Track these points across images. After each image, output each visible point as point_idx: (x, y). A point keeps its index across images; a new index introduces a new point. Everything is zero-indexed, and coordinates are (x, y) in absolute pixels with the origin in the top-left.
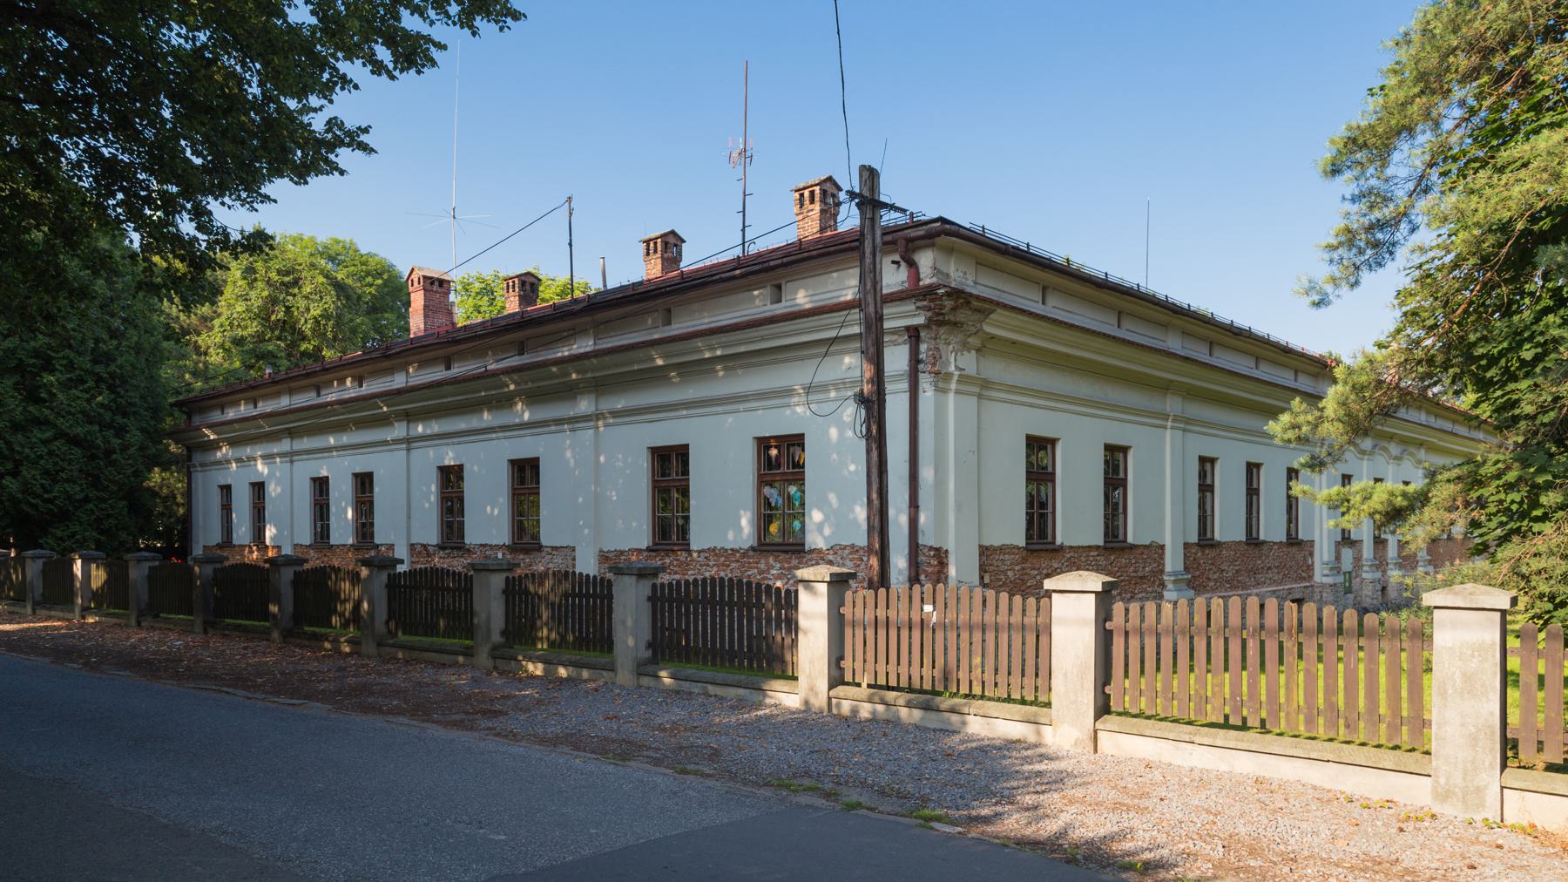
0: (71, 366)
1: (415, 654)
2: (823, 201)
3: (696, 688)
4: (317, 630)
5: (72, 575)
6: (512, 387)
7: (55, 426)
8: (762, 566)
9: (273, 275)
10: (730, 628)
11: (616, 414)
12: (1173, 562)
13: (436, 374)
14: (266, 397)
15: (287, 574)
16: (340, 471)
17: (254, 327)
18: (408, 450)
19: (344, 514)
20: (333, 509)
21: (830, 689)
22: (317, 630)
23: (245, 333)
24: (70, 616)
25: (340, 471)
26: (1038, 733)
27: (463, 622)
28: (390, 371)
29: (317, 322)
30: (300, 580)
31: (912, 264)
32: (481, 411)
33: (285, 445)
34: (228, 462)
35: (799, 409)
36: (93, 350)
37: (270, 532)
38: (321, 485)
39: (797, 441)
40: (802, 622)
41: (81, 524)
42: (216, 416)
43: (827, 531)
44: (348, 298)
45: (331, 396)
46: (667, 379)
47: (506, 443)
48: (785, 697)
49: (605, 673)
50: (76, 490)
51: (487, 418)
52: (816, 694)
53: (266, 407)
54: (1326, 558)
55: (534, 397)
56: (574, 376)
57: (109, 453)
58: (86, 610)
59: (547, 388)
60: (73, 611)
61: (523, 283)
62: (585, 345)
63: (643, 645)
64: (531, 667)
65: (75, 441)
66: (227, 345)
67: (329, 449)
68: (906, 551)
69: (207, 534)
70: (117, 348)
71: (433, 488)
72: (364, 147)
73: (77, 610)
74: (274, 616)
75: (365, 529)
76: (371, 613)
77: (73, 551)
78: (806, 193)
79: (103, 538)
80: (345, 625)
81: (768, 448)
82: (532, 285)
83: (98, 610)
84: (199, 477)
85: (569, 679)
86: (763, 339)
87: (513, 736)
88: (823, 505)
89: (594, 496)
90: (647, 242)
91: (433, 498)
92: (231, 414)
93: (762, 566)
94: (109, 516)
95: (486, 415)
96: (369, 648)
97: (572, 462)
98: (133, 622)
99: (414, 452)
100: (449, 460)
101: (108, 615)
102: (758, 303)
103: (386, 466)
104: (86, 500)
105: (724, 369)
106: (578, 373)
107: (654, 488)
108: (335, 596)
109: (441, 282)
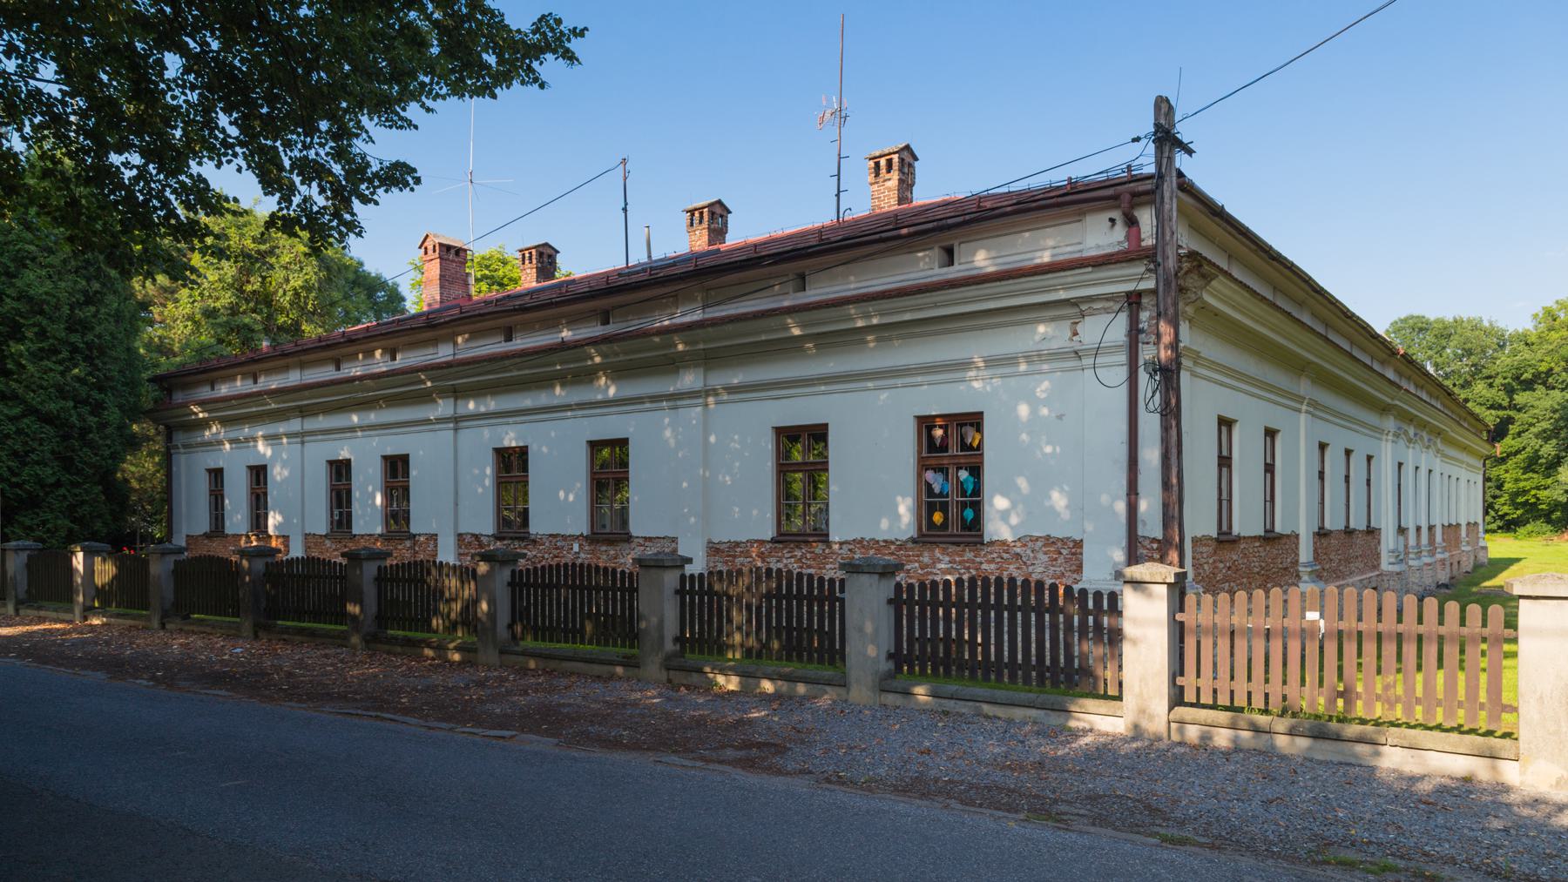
0: (42, 334)
1: (553, 664)
2: (901, 170)
3: (965, 708)
4: (409, 634)
5: (70, 570)
6: (598, 360)
7: (24, 402)
8: (926, 559)
9: (249, 243)
10: (1040, 637)
11: (731, 390)
12: (1305, 553)
13: (493, 346)
14: (269, 372)
15: (370, 569)
16: (365, 454)
17: (227, 298)
18: (456, 430)
19: (370, 502)
20: (356, 494)
21: (1170, 709)
22: (409, 634)
23: (218, 305)
24: (68, 616)
25: (365, 454)
26: (1494, 768)
27: (622, 627)
28: (435, 342)
29: (297, 294)
30: (384, 578)
31: (1131, 222)
32: (552, 387)
33: (295, 425)
34: (220, 443)
35: (976, 385)
36: (70, 317)
37: (274, 520)
38: (340, 470)
39: (975, 420)
40: (1128, 628)
41: (52, 510)
42: (205, 393)
43: (1014, 520)
44: (328, 269)
45: (354, 370)
46: (801, 350)
47: (585, 421)
48: (1099, 721)
49: (828, 688)
50: (48, 473)
51: (559, 394)
52: (1151, 718)
53: (273, 382)
54: (1391, 546)
55: (619, 372)
56: (680, 347)
57: (85, 431)
58: (88, 610)
59: (642, 360)
60: (71, 611)
61: (541, 255)
62: (689, 314)
63: (883, 656)
64: (721, 679)
65: (47, 419)
66: (198, 317)
67: (352, 429)
68: (1124, 543)
69: (192, 519)
70: (94, 316)
71: (489, 471)
72: (570, 57)
73: (77, 611)
74: (354, 617)
75: (397, 515)
76: (492, 615)
77: (74, 542)
78: (883, 162)
79: (76, 527)
80: (452, 627)
81: (930, 429)
82: (550, 256)
83: (102, 611)
84: (181, 461)
85: (777, 696)
86: (936, 306)
87: (780, 772)
88: (1008, 490)
89: (702, 477)
90: (692, 212)
91: (488, 482)
92: (224, 390)
93: (926, 559)
94: (83, 502)
95: (558, 390)
96: (490, 656)
97: (672, 442)
98: (156, 624)
99: (463, 434)
100: (510, 440)
101: (118, 616)
102: (924, 267)
103: (427, 449)
104: (58, 484)
105: (878, 340)
106: (686, 343)
107: (593, 479)
108: (439, 593)
109: (459, 251)
